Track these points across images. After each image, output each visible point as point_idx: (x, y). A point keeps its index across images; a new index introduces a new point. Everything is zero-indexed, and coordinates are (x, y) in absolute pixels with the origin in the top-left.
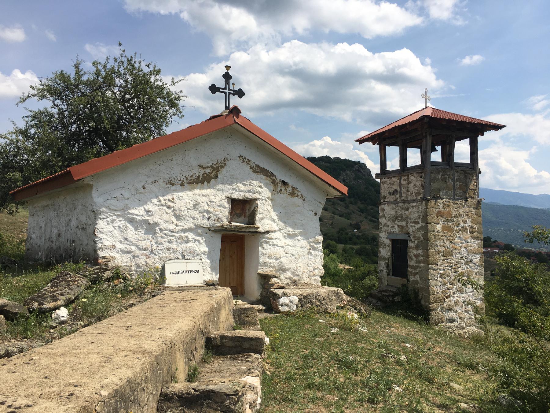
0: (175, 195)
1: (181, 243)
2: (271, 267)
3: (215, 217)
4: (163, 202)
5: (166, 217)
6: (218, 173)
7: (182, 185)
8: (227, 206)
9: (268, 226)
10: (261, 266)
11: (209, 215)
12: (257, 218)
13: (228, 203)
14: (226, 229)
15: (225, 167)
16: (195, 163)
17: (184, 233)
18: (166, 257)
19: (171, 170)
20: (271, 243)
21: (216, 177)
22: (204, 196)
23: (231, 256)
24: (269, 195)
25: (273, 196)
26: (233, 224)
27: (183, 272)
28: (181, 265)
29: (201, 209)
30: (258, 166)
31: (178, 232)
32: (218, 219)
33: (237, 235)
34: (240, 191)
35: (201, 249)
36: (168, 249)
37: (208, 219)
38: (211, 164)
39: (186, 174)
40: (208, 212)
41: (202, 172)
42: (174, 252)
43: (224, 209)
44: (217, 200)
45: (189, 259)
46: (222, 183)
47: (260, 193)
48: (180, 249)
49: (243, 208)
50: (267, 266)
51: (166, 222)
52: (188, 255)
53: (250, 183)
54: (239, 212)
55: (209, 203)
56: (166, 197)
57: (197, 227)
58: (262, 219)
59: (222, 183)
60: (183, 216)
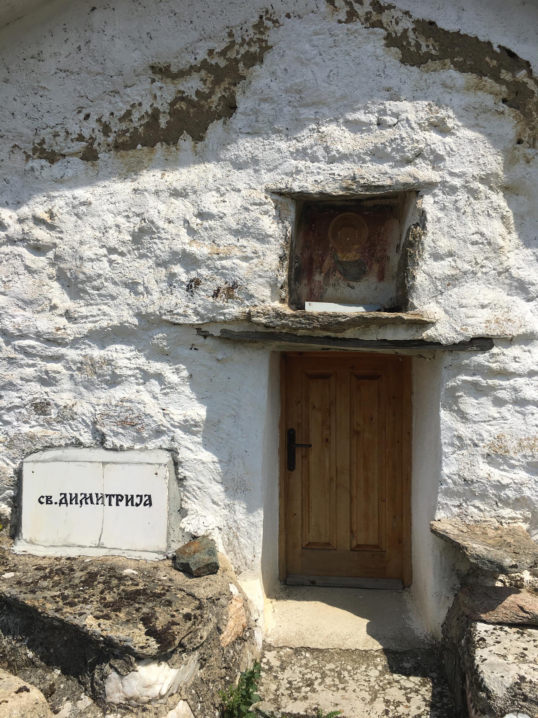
0: (62, 200)
1: (89, 386)
2: (506, 502)
3: (220, 282)
4: (15, 229)
5: (24, 285)
6: (238, 90)
7: (90, 155)
8: (273, 227)
9: (486, 314)
10: (449, 493)
11: (193, 275)
12: (420, 279)
13: (280, 218)
14: (290, 335)
15: (268, 57)
16: (130, 57)
17: (103, 347)
18: (32, 438)
19: (37, 100)
20: (502, 394)
21: (230, 107)
22: (176, 194)
23: (355, 433)
24: (494, 162)
25: (520, 169)
26: (314, 308)
27: (88, 498)
28: (84, 472)
29: (161, 248)
30: (427, 28)
31: (75, 343)
32: (231, 290)
33: (384, 358)
34: (334, 158)
35: (171, 409)
36: (41, 408)
37: (189, 288)
38: (202, 55)
39: (104, 109)
40: (189, 260)
41: (167, 92)
42: (62, 419)
43: (258, 246)
44: (229, 207)
45: (121, 449)
46: (253, 133)
47: (436, 160)
48: (84, 409)
49: (354, 233)
50: (483, 497)
51: (26, 303)
52: (116, 434)
53: (383, 112)
54: (352, 256)
55: (195, 222)
56: (25, 210)
57: (150, 322)
58: (452, 281)
59: (253, 133)
60: (90, 279)
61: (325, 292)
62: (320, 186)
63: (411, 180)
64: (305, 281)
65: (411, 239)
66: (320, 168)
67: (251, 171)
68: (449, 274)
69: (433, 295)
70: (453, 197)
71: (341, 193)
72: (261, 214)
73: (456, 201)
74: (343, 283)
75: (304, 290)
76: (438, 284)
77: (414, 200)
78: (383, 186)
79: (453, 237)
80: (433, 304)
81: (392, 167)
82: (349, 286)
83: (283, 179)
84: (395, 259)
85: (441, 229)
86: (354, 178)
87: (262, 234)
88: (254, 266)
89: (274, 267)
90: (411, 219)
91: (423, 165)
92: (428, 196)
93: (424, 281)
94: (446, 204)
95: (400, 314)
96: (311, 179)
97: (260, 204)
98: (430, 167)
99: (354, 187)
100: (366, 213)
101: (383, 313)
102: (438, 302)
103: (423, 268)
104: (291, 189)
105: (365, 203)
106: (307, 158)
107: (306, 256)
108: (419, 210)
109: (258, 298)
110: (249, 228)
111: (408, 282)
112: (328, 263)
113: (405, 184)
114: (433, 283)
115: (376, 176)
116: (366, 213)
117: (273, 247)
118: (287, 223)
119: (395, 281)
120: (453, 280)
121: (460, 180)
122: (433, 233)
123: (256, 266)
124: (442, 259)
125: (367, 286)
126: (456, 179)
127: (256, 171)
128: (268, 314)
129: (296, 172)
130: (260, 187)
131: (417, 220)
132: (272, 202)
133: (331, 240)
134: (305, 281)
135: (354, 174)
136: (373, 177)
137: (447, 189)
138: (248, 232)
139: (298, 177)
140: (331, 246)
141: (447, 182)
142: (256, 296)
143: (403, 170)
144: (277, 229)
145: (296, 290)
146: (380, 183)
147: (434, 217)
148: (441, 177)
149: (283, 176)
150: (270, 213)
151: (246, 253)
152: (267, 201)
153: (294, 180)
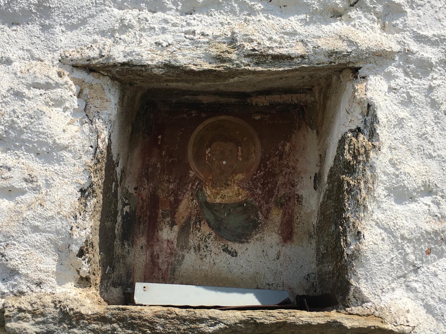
13: (87, 113)
26: (152, 297)
43: (37, 167)
61: (180, 262)
62: (165, 53)
63: (342, 47)
64: (142, 241)
65: (348, 157)
66: (166, 21)
67: (35, 28)
68: (429, 230)
69: (400, 273)
70: (423, 81)
71: (207, 66)
72: (47, 104)
73: (431, 89)
74: (214, 246)
75: (139, 258)
76: (409, 251)
77: (349, 86)
78: (289, 58)
79: (430, 157)
80: (400, 292)
81: (306, 23)
82: (225, 250)
83: (95, 41)
84: (312, 201)
85: (405, 140)
86: (232, 41)
87: (47, 144)
88: (24, 207)
89: (66, 210)
90: (345, 121)
91: (365, 20)
92: (378, 78)
93: (379, 242)
94: (413, 94)
95: (334, 315)
96: (148, 41)
97: (47, 86)
98: (377, 26)
99: (233, 56)
100: (258, 118)
101: (299, 313)
102: (409, 288)
103: (375, 217)
104: (109, 57)
105: (255, 100)
106: (143, 5)
107: (145, 193)
108: (360, 102)
109: (26, 276)
110: (21, 132)
111: (348, 245)
112: (186, 206)
113: (331, 53)
114: (398, 247)
115: (275, 37)
116: (258, 118)
117: (68, 170)
118: (99, 124)
119: (314, 242)
120: (436, 242)
121: (435, 50)
122: (390, 148)
123: (29, 207)
124: (412, 199)
125: (260, 252)
126: (428, 48)
127: (45, 28)
128: (42, 315)
129: (121, 28)
130: (50, 56)
131: (358, 122)
132: (71, 82)
133: (192, 164)
134: (142, 241)
135: (233, 33)
136: (270, 39)
137: (413, 66)
138: (17, 139)
139: (123, 37)
140: (192, 174)
141: (413, 53)
142: (24, 271)
143: (326, 28)
144: (78, 134)
145: (124, 257)
146: (284, 51)
147: (391, 117)
148: (399, 43)
149: (96, 37)
150: (67, 104)
151: (10, 181)
152: (60, 81)
153: (116, 42)
